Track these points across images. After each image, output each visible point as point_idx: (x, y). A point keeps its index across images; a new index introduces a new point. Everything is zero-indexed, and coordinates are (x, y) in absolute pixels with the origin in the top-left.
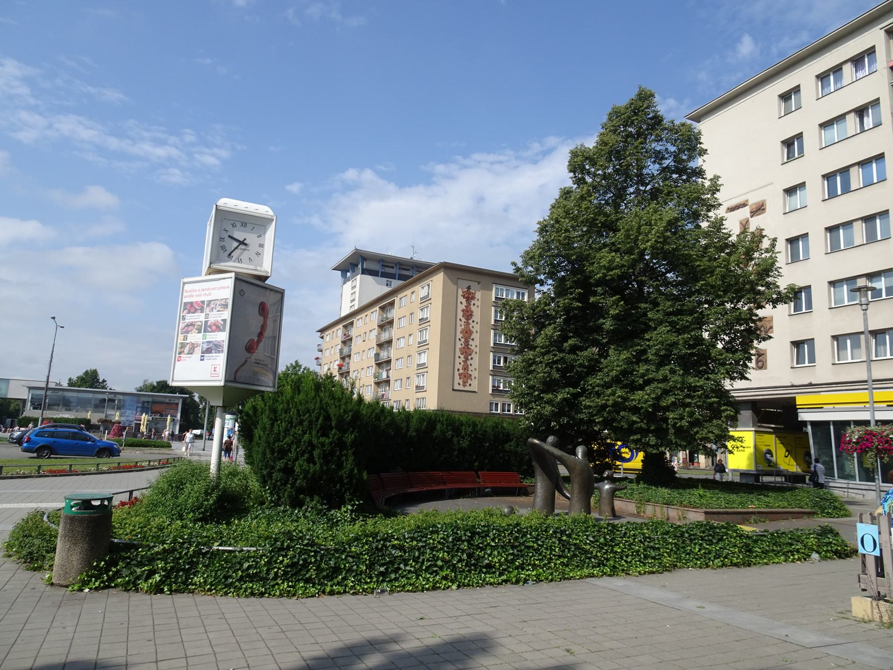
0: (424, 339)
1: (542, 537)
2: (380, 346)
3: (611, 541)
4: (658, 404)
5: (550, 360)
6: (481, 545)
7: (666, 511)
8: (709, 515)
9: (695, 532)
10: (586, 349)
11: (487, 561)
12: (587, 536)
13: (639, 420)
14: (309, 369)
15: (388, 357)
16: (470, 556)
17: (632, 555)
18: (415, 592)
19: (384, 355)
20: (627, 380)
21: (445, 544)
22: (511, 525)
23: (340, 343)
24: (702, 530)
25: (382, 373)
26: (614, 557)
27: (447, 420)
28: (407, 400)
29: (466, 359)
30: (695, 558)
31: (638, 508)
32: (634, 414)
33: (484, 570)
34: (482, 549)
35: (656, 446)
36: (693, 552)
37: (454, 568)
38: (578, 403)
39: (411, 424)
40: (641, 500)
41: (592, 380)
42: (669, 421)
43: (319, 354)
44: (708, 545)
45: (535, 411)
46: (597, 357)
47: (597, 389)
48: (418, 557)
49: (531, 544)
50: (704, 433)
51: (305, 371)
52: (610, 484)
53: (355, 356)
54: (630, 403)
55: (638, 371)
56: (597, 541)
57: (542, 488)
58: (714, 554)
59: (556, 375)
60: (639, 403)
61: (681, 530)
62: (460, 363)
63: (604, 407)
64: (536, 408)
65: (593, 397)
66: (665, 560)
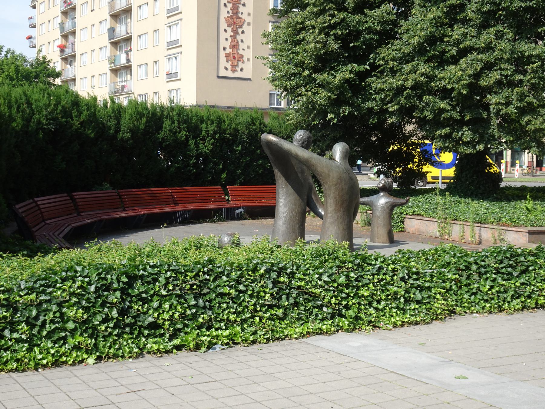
0: (175, 5)
1: (247, 279)
2: (115, 16)
3: (356, 280)
4: (477, 83)
5: (325, 23)
6: (144, 295)
7: (478, 232)
8: (535, 236)
9: (487, 263)
10: (379, 7)
11: (151, 319)
12: (321, 274)
13: (449, 107)
14: (13, 52)
15: (127, 33)
16: (123, 312)
17: (387, 300)
18: (24, 371)
19: (121, 31)
20: (434, 50)
21: (84, 295)
22: (199, 263)
23: (60, 14)
24: (500, 258)
25: (120, 55)
26: (359, 303)
27: (179, 115)
28: (156, 93)
29: (236, 33)
30: (483, 299)
31: (442, 228)
32: (443, 99)
33: (146, 332)
34: (145, 301)
35: (471, 143)
36: (481, 291)
37: (94, 333)
38: (365, 86)
39: (122, 122)
40: (446, 218)
41: (385, 52)
42: (491, 107)
43: (32, 32)
44: (504, 280)
45: (305, 99)
46: (394, 17)
47: (391, 64)
48: (36, 318)
49: (227, 290)
50: (538, 123)
51: (9, 56)
52: (387, 197)
53: (82, 32)
54: (437, 83)
55: (451, 36)
56: (335, 281)
57: (285, 206)
58: (513, 293)
59: (334, 46)
60: (449, 83)
61: (468, 259)
62: (227, 39)
63: (400, 90)
64: (306, 94)
65: (387, 76)
66: (436, 305)
